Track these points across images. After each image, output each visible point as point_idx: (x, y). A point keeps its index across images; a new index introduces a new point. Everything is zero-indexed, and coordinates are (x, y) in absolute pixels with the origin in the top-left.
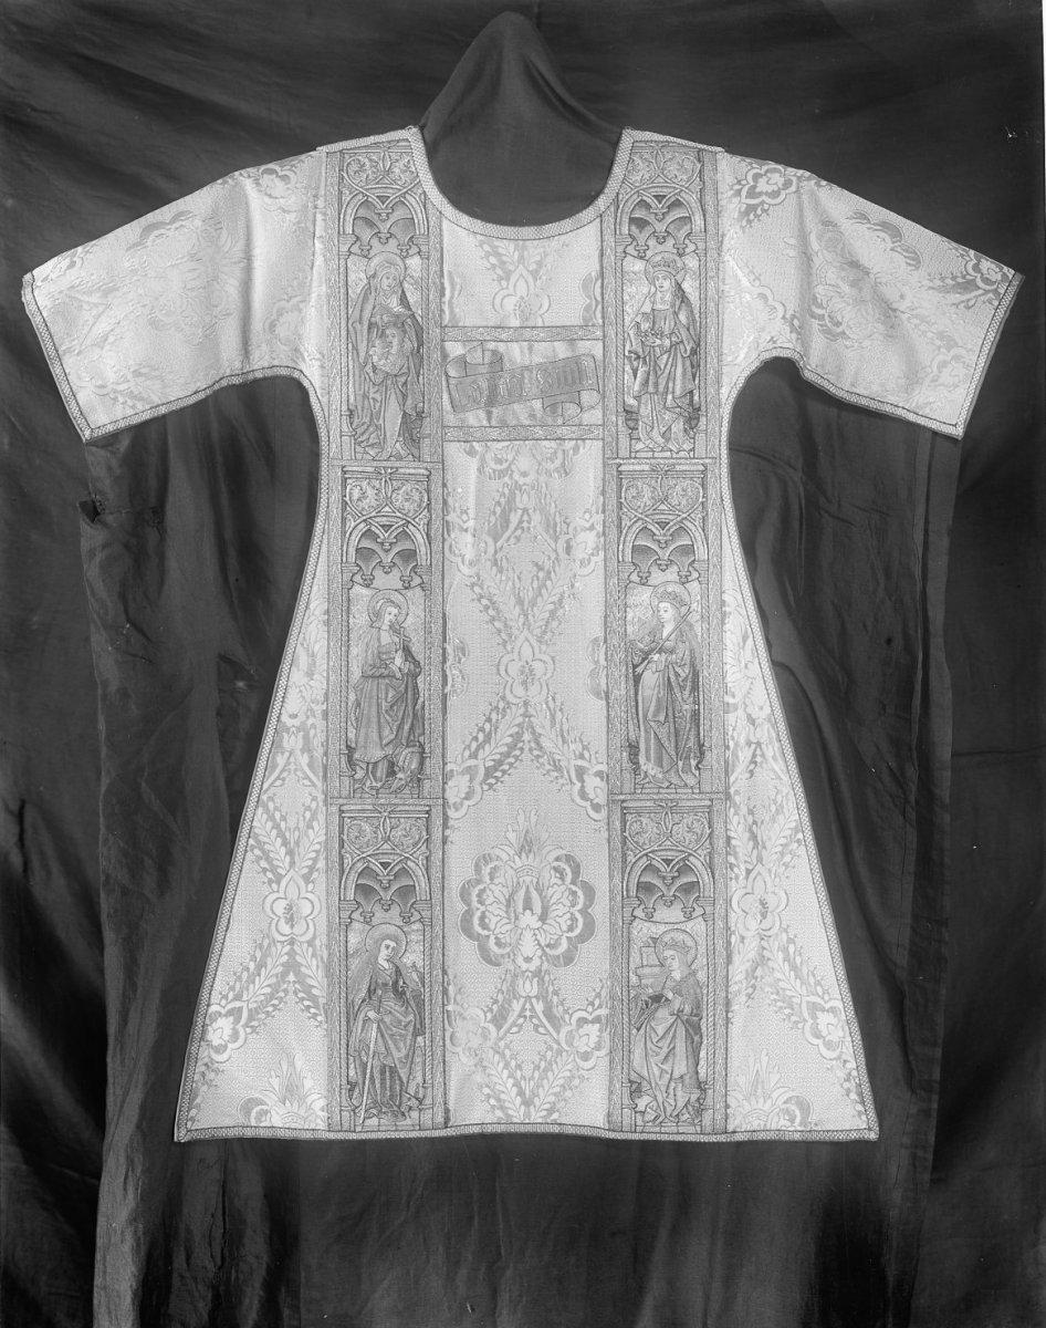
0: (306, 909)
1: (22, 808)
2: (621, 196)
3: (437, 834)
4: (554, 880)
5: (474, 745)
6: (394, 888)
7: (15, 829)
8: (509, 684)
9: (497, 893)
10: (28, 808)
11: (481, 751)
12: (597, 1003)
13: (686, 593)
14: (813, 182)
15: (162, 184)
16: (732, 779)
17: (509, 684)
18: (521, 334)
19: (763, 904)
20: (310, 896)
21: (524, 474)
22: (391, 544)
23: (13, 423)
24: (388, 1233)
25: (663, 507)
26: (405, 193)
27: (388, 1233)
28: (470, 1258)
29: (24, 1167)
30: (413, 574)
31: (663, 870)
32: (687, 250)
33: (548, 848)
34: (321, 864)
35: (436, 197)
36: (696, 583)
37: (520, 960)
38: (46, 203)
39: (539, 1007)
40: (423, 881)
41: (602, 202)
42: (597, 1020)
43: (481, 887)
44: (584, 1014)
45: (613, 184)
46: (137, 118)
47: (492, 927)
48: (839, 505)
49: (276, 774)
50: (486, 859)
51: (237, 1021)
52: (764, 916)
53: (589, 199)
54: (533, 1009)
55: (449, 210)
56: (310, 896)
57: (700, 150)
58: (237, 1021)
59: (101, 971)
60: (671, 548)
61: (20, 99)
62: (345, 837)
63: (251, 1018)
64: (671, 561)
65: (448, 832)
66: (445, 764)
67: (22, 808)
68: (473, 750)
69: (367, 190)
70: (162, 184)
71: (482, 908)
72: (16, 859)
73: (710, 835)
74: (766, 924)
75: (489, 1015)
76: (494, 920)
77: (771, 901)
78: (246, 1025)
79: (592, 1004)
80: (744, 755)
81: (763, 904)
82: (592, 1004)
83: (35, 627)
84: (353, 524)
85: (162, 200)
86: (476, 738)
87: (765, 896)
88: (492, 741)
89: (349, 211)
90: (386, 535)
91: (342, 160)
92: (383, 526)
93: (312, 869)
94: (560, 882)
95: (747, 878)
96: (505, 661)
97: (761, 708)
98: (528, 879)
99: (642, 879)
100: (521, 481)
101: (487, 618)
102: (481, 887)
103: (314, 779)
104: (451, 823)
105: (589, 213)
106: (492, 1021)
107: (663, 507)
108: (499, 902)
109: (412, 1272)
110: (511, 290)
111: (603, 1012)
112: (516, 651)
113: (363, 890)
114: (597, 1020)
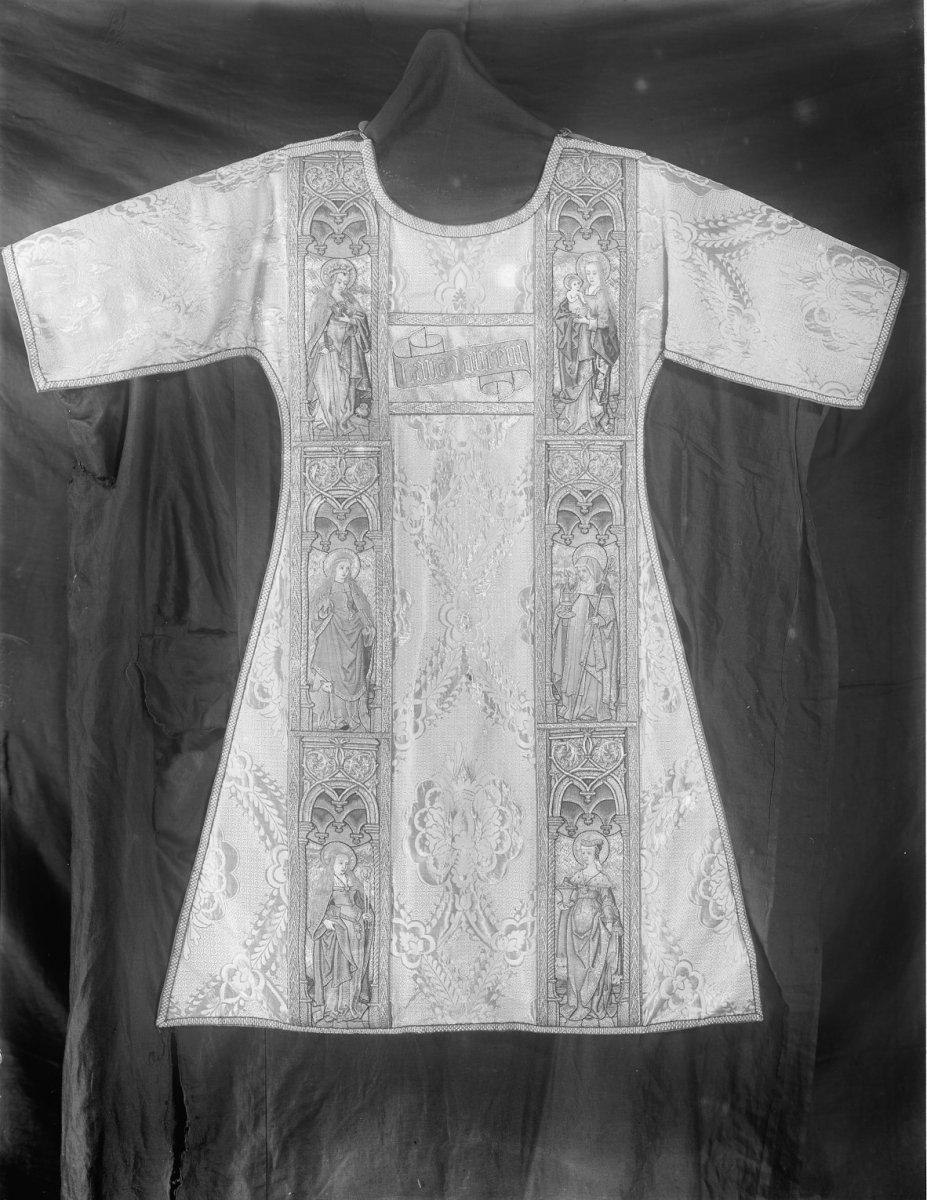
2: (551, 197)
3: (385, 766)
9: (437, 817)
12: (523, 912)
18: (458, 319)
22: (342, 218)
25: (586, 477)
32: (608, 542)
35: (380, 195)
37: (454, 445)
40: (373, 806)
41: (535, 202)
42: (523, 927)
43: (422, 811)
44: (512, 922)
45: (544, 185)
47: (431, 848)
50: (429, 785)
57: (622, 160)
60: (595, 218)
62: (304, 766)
63: (217, 988)
65: (395, 762)
70: (133, 182)
71: (423, 831)
73: (624, 759)
75: (429, 929)
78: (222, 982)
79: (519, 913)
80: (649, 799)
82: (519, 913)
83: (19, 577)
84: (312, 497)
85: (130, 194)
90: (341, 507)
92: (337, 499)
96: (441, 288)
102: (422, 811)
104: (398, 754)
105: (523, 213)
106: (432, 934)
107: (586, 477)
111: (529, 919)
112: (452, 279)
113: (319, 814)
114: (523, 927)
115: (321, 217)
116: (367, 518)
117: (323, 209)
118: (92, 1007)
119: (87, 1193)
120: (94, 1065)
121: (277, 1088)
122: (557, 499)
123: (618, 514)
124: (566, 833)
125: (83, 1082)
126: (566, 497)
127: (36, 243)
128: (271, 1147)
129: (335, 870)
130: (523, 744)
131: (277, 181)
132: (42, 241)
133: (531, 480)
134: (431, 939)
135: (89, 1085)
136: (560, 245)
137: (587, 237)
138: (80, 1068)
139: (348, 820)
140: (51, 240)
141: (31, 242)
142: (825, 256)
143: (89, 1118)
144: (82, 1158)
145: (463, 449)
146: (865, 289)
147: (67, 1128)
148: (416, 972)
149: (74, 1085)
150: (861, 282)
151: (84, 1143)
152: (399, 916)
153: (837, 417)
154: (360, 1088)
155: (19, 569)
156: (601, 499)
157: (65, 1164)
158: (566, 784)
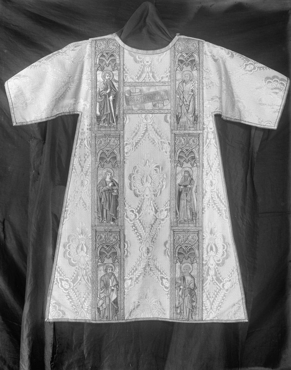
0: (86, 183)
1: (4, 221)
4: (155, 173)
5: (133, 271)
6: (110, 59)
7: (2, 227)
8: (142, 254)
10: (6, 221)
11: (135, 273)
12: (166, 205)
13: (191, 171)
14: (225, 208)
15: (49, 47)
16: (204, 285)
17: (142, 254)
19: (211, 182)
20: (87, 179)
21: (147, 62)
23: (5, 113)
24: (108, 344)
26: (114, 149)
27: (108, 344)
28: (131, 352)
29: (2, 321)
30: (116, 259)
31: (186, 153)
33: (152, 299)
34: (90, 170)
36: (196, 264)
38: (16, 51)
39: (151, 75)
46: (42, 28)
48: (231, 142)
49: (78, 282)
51: (63, 280)
52: (212, 186)
53: (164, 45)
54: (149, 75)
55: (126, 47)
56: (87, 179)
58: (63, 280)
59: (26, 268)
61: (9, 22)
62: (96, 143)
64: (189, 257)
66: (124, 277)
67: (4, 221)
68: (132, 273)
69: (103, 244)
72: (2, 236)
74: (212, 188)
76: (138, 185)
77: (214, 182)
81: (211, 182)
83: (9, 170)
84: (98, 246)
86: (133, 269)
87: (213, 180)
88: (138, 270)
89: (98, 57)
91: (96, 43)
93: (87, 172)
94: (156, 173)
95: (207, 175)
97: (212, 265)
98: (83, 242)
99: (180, 155)
100: (147, 64)
101: (137, 236)
103: (88, 147)
106: (138, 212)
108: (139, 180)
109: (115, 355)
110: (142, 119)
115: (101, 58)
116: (116, 59)
117: (103, 56)
118: (30, 305)
119: (28, 363)
120: (31, 323)
121: (87, 335)
122: (178, 153)
123: (197, 59)
124: (179, 69)
125: (27, 328)
126: (180, 248)
127: (12, 80)
128: (85, 353)
129: (106, 175)
130: (166, 154)
131: (88, 47)
132: (14, 79)
133: (169, 206)
134: (137, 214)
135: (29, 329)
136: (179, 165)
137: (187, 66)
138: (26, 324)
139: (111, 62)
140: (17, 79)
141: (11, 80)
142: (264, 81)
143: (29, 339)
144: (27, 352)
145: (147, 197)
146: (277, 91)
147: (22, 342)
148: (133, 225)
149: (24, 329)
150: (275, 88)
151: (27, 347)
152: (127, 73)
153: (267, 132)
154: (113, 334)
155: (9, 168)
156: (192, 249)
157: (21, 354)
158: (180, 150)
